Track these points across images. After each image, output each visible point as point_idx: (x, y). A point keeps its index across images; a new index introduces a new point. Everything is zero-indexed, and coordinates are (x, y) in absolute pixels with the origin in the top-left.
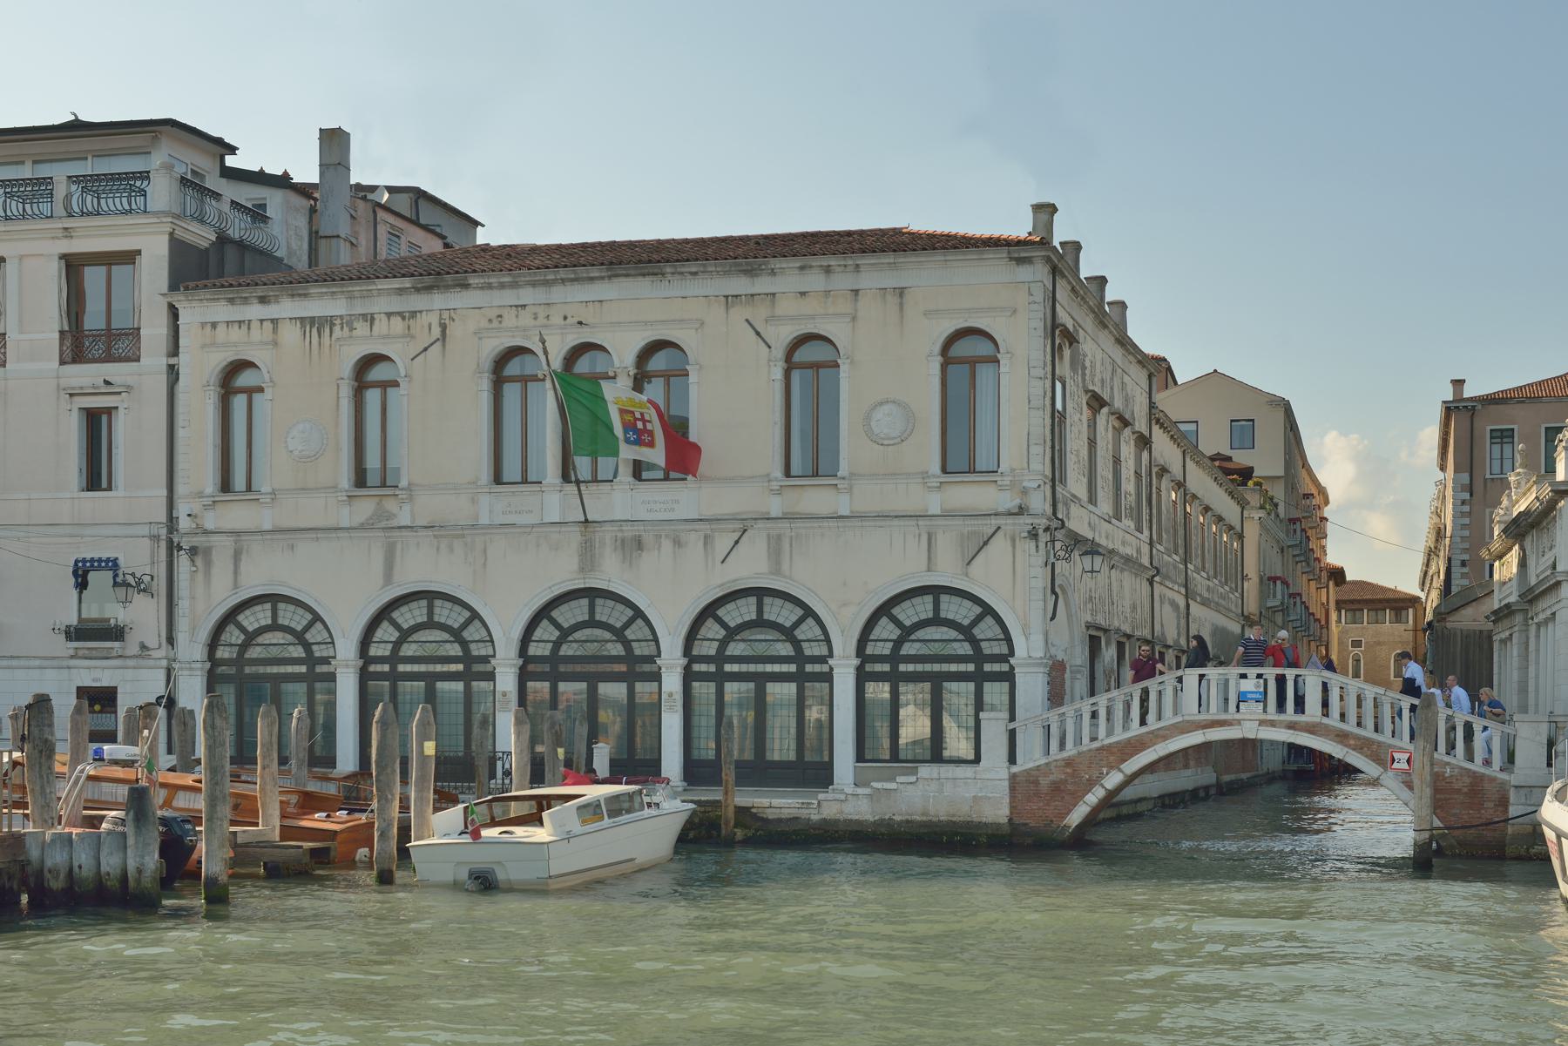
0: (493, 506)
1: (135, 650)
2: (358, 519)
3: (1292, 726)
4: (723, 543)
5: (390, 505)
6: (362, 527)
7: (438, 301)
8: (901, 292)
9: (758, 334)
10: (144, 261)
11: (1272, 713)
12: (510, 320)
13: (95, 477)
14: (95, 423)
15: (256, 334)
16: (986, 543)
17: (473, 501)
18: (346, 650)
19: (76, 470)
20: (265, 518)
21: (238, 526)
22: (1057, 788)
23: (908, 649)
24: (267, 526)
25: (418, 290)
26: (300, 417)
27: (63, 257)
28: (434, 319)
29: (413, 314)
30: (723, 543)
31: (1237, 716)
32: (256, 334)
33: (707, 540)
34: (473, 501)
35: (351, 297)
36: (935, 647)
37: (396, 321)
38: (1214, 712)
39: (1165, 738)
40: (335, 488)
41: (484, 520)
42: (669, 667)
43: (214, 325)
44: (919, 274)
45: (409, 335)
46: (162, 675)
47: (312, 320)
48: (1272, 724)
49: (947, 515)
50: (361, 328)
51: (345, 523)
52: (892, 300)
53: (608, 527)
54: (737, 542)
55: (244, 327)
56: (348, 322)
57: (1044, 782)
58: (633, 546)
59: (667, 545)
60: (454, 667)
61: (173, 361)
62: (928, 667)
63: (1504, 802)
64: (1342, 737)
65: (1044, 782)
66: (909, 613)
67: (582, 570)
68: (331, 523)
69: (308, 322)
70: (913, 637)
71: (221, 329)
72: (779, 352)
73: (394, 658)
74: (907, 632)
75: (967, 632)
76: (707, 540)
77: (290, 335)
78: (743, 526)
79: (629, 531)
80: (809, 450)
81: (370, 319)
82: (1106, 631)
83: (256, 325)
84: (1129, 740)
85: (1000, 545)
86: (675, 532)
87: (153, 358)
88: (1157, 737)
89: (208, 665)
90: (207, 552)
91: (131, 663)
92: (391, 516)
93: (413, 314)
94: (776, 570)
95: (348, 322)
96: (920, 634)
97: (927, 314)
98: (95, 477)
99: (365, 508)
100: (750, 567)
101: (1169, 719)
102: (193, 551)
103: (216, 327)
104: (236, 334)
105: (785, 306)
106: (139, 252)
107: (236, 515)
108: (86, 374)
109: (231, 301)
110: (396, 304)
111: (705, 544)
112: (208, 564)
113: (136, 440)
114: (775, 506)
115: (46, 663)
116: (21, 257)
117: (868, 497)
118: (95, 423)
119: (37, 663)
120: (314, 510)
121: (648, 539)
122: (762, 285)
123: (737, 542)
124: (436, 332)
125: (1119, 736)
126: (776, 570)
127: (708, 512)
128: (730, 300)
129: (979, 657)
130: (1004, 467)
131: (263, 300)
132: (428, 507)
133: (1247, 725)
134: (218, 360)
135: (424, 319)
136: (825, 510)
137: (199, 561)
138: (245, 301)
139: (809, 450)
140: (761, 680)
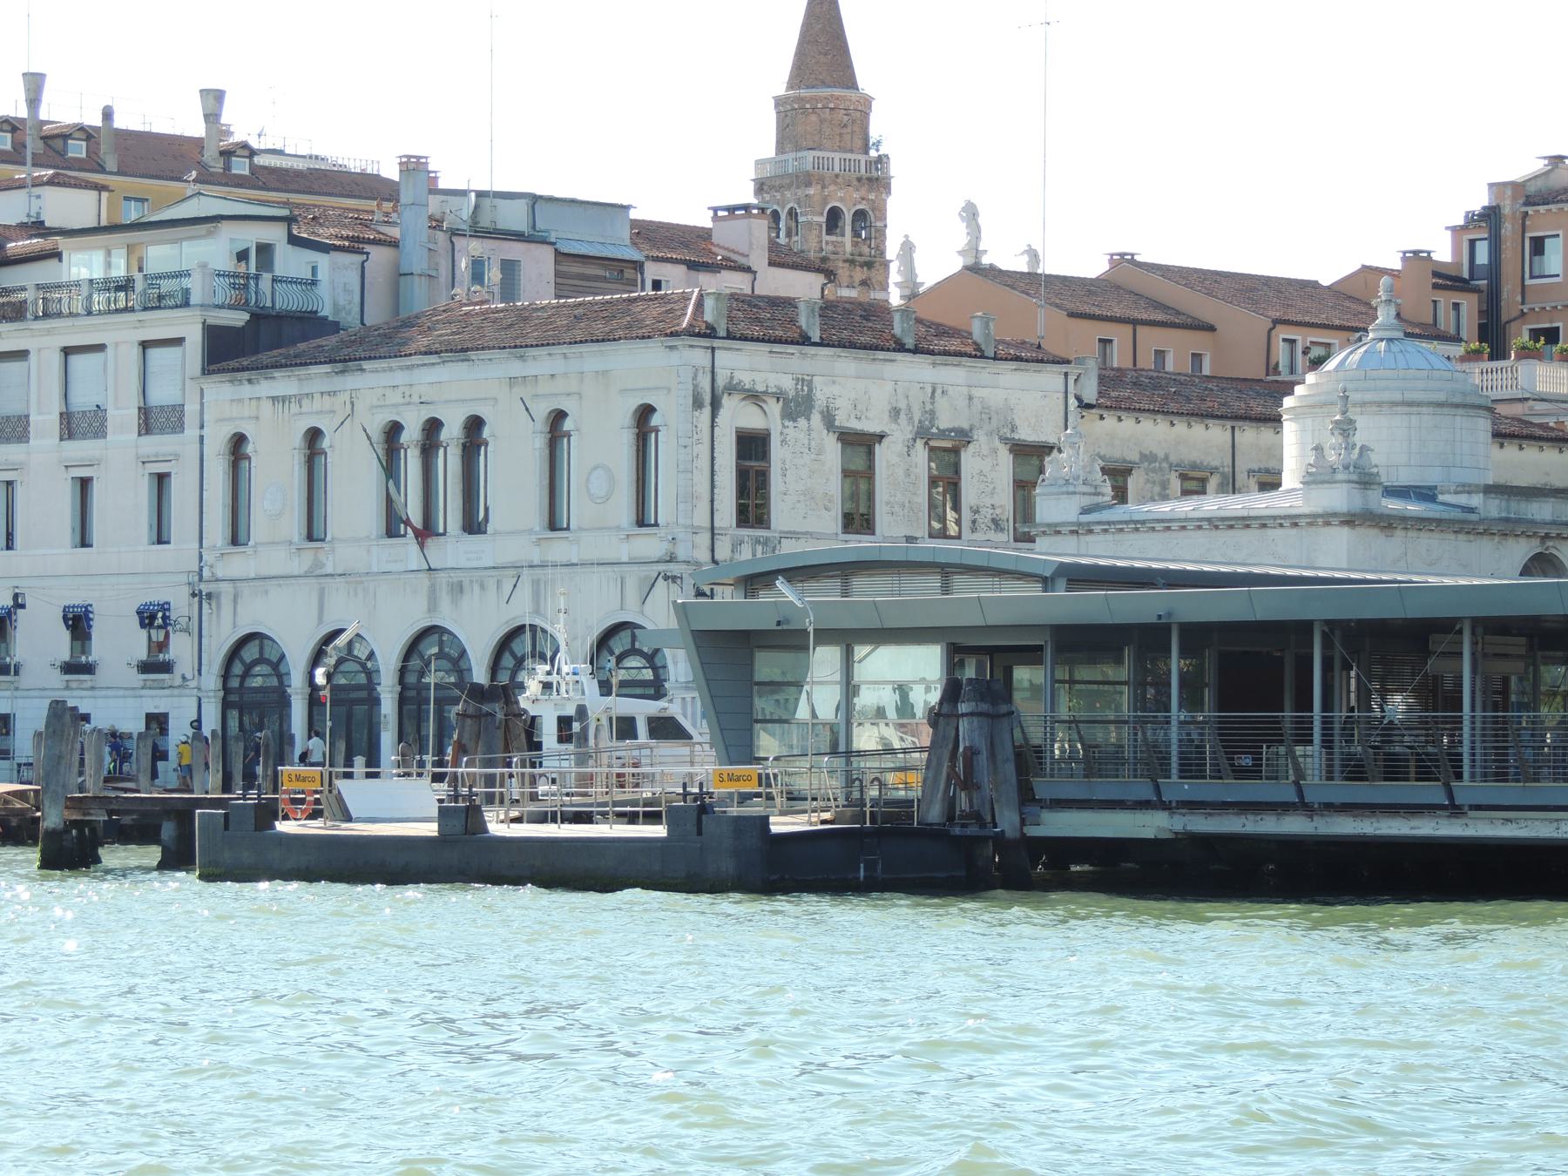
1: (178, 681)
8: (605, 373)
10: (187, 342)
19: (69, 530)
53: (442, 574)
56: (299, 399)
59: (476, 588)
69: (274, 399)
77: (267, 407)
79: (456, 577)
87: (191, 432)
89: (221, 694)
90: (218, 596)
91: (176, 692)
94: (537, 612)
95: (299, 399)
98: (161, 539)
102: (209, 596)
103: (230, 403)
108: (80, 449)
116: (117, 344)
119: (121, 693)
121: (466, 584)
124: (349, 406)
127: (500, 561)
128: (512, 381)
134: (227, 431)
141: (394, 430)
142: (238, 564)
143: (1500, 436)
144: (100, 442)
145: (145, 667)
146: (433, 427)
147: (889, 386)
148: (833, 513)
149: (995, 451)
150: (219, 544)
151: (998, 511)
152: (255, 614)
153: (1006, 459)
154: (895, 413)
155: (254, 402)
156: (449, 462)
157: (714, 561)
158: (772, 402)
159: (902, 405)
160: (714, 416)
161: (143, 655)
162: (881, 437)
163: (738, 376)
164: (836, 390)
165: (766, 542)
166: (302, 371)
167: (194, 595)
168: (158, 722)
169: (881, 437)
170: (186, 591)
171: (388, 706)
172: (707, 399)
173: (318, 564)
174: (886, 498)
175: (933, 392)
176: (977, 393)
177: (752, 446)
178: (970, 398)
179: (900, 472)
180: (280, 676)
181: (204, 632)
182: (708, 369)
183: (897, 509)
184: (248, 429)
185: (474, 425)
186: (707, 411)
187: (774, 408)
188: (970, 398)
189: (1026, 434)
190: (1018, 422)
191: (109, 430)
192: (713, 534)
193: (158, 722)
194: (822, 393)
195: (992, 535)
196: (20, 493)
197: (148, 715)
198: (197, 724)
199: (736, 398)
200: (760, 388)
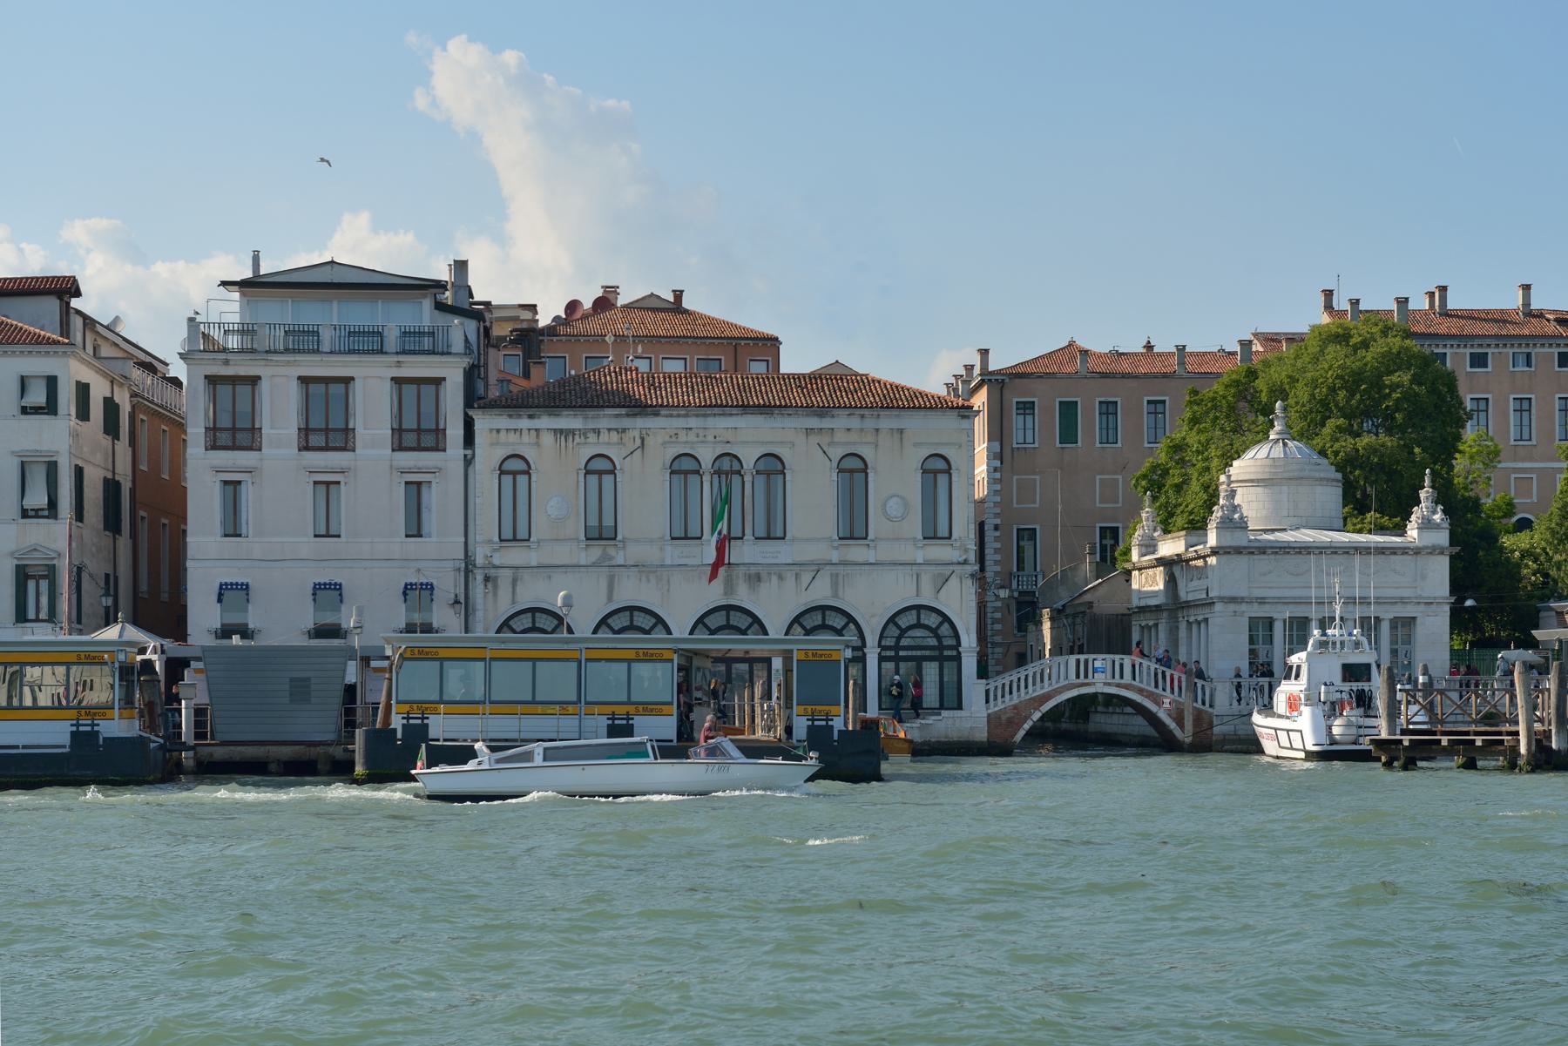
0: (675, 553)
2: (593, 559)
3: (1118, 686)
4: (806, 578)
5: (612, 551)
6: (594, 565)
7: (640, 422)
8: (901, 431)
11: (1117, 679)
12: (682, 437)
13: (415, 529)
14: (415, 489)
15: (525, 438)
17: (661, 549)
20: (533, 558)
21: (517, 562)
22: (1010, 721)
23: (904, 642)
24: (534, 563)
25: (628, 415)
26: (557, 498)
28: (636, 434)
29: (624, 430)
30: (806, 578)
32: (525, 438)
33: (797, 576)
34: (661, 549)
35: (586, 418)
36: (918, 639)
37: (614, 434)
40: (577, 539)
41: (668, 562)
43: (498, 431)
44: (913, 423)
45: (621, 443)
47: (561, 431)
49: (927, 563)
50: (592, 438)
51: (583, 562)
52: (897, 436)
56: (584, 433)
57: (1004, 718)
58: (755, 579)
59: (774, 579)
61: (469, 452)
62: (914, 653)
63: (1211, 726)
64: (1140, 691)
65: (1004, 718)
66: (904, 622)
67: (725, 594)
68: (574, 562)
69: (558, 432)
71: (503, 434)
72: (835, 465)
74: (903, 631)
75: (934, 631)
76: (797, 576)
77: (548, 439)
78: (818, 567)
79: (753, 570)
80: (854, 528)
81: (597, 432)
85: (954, 581)
86: (779, 571)
90: (496, 578)
92: (612, 558)
93: (624, 430)
94: (835, 595)
95: (584, 433)
96: (910, 633)
97: (916, 445)
98: (415, 529)
99: (595, 552)
100: (820, 593)
101: (1063, 683)
103: (497, 434)
104: (512, 437)
105: (840, 437)
106: (444, 379)
107: (515, 556)
109: (510, 416)
110: (614, 424)
112: (496, 587)
113: (442, 501)
114: (835, 556)
117: (884, 552)
118: (415, 489)
120: (563, 554)
121: (764, 576)
122: (826, 423)
126: (835, 595)
127: (798, 559)
129: (941, 647)
130: (955, 535)
131: (531, 417)
132: (633, 553)
135: (630, 434)
136: (861, 559)
137: (490, 585)
138: (520, 416)
139: (854, 528)
143: (66, 289)
166: (591, 412)
171: (969, 641)
173: (605, 557)
196: (248, 494)
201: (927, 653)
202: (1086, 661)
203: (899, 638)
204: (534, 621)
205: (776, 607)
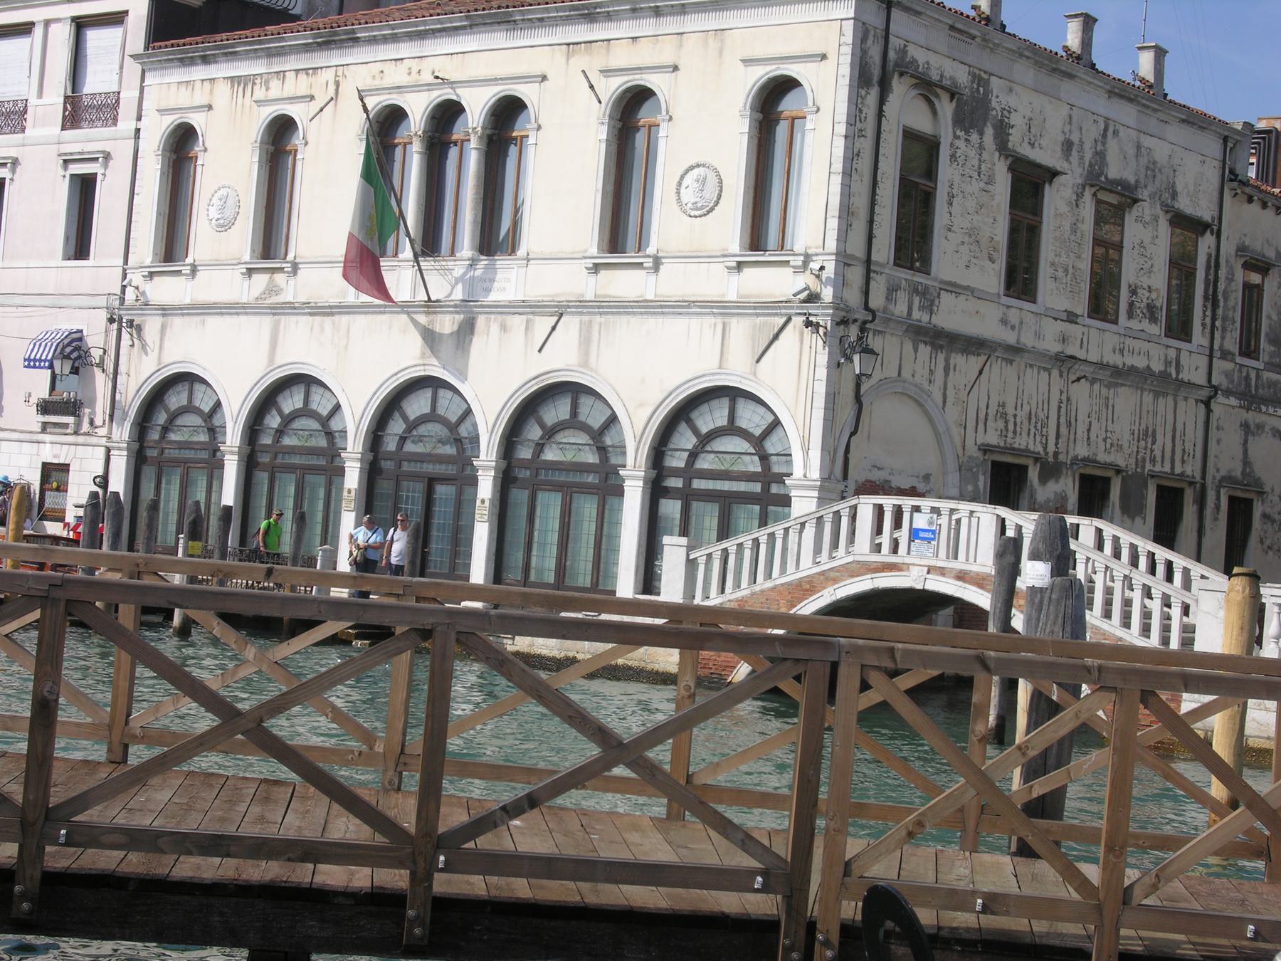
9: (592, 87)
10: (130, 19)
13: (79, 246)
14: (84, 189)
16: (776, 337)
18: (233, 437)
23: (705, 463)
27: (74, 19)
31: (907, 560)
38: (885, 556)
39: (835, 581)
42: (486, 468)
46: (101, 452)
48: (942, 571)
54: (554, 328)
55: (190, 88)
60: (591, 479)
70: (708, 448)
73: (689, 472)
74: (705, 440)
77: (223, 89)
82: (1118, 472)
83: (198, 84)
84: (800, 581)
87: (126, 124)
88: (827, 579)
94: (585, 363)
95: (266, 79)
98: (79, 246)
101: (842, 558)
106: (126, 12)
111: (527, 328)
115: (22, 436)
116: (47, 23)
117: (674, 281)
118: (84, 189)
119: (15, 436)
123: (554, 328)
124: (332, 88)
125: (792, 576)
126: (585, 363)
133: (915, 571)
134: (169, 121)
140: (431, 482)
141: (390, 119)
142: (167, 290)
144: (17, 137)
145: (45, 407)
146: (448, 113)
147: (1065, 110)
148: (996, 266)
149: (1156, 219)
150: (148, 261)
151: (1154, 295)
152: (182, 347)
153: (1164, 227)
154: (1068, 146)
155: (207, 84)
156: (468, 166)
157: (867, 308)
158: (945, 97)
159: (1075, 138)
160: (882, 101)
161: (44, 393)
162: (1053, 174)
163: (913, 52)
164: (1012, 101)
165: (922, 292)
167: (111, 320)
168: (54, 474)
169: (1053, 174)
170: (104, 315)
172: (876, 72)
173: (272, 290)
174: (1051, 257)
175: (1106, 130)
176: (1147, 141)
177: (922, 154)
178: (1139, 147)
179: (1067, 225)
180: (212, 431)
181: (122, 368)
182: (880, 33)
183: (1060, 274)
184: (196, 120)
185: (508, 111)
186: (874, 93)
187: (946, 108)
188: (1139, 147)
189: (1185, 205)
190: (1179, 188)
191: (29, 124)
192: (868, 271)
193: (54, 474)
194: (1000, 97)
195: (1146, 325)
197: (45, 465)
198: (104, 481)
199: (908, 81)
200: (935, 77)
201: (742, 487)
202: (898, 512)
203: (693, 455)
204: (695, 431)
205: (490, 387)
